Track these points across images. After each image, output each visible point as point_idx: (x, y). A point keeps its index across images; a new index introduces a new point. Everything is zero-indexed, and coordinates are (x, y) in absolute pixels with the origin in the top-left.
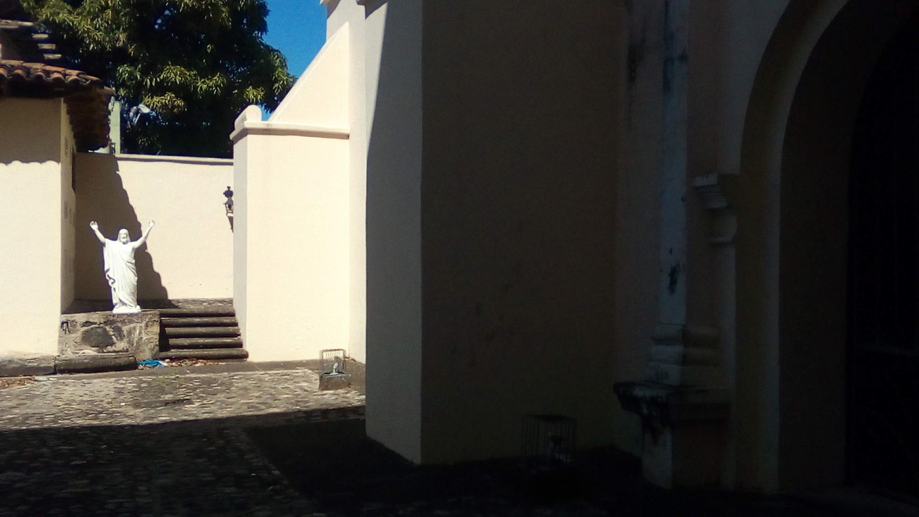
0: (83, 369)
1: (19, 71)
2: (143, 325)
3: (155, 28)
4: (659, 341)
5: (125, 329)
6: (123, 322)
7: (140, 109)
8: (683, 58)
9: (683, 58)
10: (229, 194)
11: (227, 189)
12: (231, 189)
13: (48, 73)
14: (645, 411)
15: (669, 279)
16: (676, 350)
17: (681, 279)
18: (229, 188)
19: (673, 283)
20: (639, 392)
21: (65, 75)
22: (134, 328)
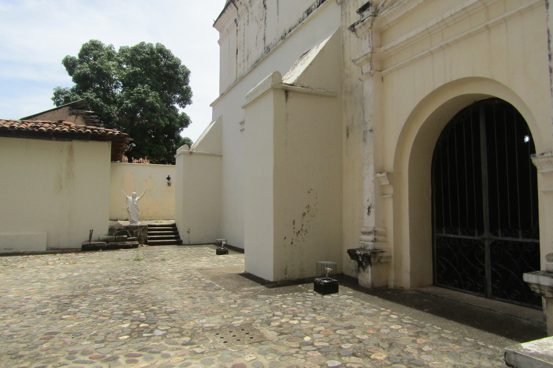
0: (214, 243)
1: (96, 131)
2: (141, 230)
3: (523, 138)
4: (364, 233)
5: (135, 231)
6: (134, 229)
7: (132, 145)
8: (371, 131)
9: (371, 131)
10: (169, 178)
11: (168, 177)
12: (170, 177)
13: (107, 131)
14: (361, 260)
15: (367, 210)
16: (371, 237)
17: (372, 210)
18: (169, 176)
19: (369, 212)
20: (358, 253)
21: (114, 132)
22: (138, 231)
